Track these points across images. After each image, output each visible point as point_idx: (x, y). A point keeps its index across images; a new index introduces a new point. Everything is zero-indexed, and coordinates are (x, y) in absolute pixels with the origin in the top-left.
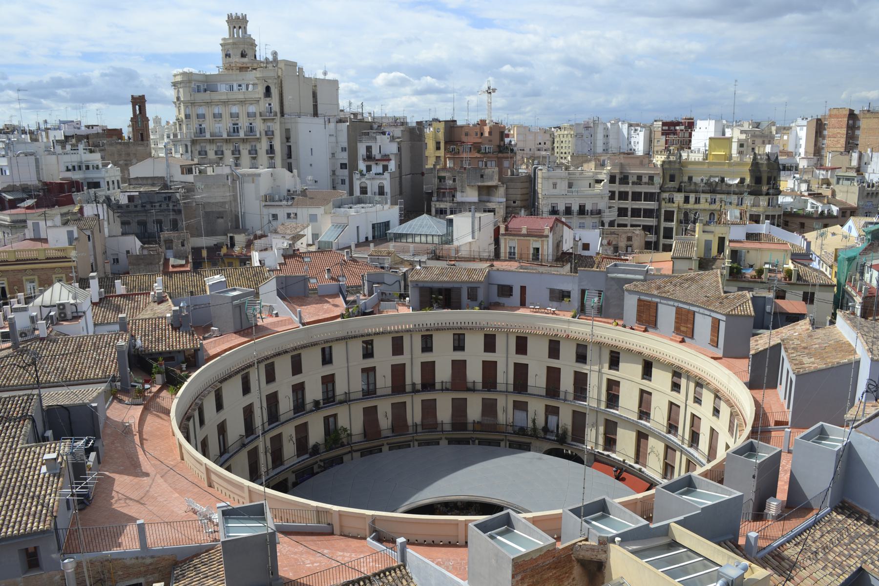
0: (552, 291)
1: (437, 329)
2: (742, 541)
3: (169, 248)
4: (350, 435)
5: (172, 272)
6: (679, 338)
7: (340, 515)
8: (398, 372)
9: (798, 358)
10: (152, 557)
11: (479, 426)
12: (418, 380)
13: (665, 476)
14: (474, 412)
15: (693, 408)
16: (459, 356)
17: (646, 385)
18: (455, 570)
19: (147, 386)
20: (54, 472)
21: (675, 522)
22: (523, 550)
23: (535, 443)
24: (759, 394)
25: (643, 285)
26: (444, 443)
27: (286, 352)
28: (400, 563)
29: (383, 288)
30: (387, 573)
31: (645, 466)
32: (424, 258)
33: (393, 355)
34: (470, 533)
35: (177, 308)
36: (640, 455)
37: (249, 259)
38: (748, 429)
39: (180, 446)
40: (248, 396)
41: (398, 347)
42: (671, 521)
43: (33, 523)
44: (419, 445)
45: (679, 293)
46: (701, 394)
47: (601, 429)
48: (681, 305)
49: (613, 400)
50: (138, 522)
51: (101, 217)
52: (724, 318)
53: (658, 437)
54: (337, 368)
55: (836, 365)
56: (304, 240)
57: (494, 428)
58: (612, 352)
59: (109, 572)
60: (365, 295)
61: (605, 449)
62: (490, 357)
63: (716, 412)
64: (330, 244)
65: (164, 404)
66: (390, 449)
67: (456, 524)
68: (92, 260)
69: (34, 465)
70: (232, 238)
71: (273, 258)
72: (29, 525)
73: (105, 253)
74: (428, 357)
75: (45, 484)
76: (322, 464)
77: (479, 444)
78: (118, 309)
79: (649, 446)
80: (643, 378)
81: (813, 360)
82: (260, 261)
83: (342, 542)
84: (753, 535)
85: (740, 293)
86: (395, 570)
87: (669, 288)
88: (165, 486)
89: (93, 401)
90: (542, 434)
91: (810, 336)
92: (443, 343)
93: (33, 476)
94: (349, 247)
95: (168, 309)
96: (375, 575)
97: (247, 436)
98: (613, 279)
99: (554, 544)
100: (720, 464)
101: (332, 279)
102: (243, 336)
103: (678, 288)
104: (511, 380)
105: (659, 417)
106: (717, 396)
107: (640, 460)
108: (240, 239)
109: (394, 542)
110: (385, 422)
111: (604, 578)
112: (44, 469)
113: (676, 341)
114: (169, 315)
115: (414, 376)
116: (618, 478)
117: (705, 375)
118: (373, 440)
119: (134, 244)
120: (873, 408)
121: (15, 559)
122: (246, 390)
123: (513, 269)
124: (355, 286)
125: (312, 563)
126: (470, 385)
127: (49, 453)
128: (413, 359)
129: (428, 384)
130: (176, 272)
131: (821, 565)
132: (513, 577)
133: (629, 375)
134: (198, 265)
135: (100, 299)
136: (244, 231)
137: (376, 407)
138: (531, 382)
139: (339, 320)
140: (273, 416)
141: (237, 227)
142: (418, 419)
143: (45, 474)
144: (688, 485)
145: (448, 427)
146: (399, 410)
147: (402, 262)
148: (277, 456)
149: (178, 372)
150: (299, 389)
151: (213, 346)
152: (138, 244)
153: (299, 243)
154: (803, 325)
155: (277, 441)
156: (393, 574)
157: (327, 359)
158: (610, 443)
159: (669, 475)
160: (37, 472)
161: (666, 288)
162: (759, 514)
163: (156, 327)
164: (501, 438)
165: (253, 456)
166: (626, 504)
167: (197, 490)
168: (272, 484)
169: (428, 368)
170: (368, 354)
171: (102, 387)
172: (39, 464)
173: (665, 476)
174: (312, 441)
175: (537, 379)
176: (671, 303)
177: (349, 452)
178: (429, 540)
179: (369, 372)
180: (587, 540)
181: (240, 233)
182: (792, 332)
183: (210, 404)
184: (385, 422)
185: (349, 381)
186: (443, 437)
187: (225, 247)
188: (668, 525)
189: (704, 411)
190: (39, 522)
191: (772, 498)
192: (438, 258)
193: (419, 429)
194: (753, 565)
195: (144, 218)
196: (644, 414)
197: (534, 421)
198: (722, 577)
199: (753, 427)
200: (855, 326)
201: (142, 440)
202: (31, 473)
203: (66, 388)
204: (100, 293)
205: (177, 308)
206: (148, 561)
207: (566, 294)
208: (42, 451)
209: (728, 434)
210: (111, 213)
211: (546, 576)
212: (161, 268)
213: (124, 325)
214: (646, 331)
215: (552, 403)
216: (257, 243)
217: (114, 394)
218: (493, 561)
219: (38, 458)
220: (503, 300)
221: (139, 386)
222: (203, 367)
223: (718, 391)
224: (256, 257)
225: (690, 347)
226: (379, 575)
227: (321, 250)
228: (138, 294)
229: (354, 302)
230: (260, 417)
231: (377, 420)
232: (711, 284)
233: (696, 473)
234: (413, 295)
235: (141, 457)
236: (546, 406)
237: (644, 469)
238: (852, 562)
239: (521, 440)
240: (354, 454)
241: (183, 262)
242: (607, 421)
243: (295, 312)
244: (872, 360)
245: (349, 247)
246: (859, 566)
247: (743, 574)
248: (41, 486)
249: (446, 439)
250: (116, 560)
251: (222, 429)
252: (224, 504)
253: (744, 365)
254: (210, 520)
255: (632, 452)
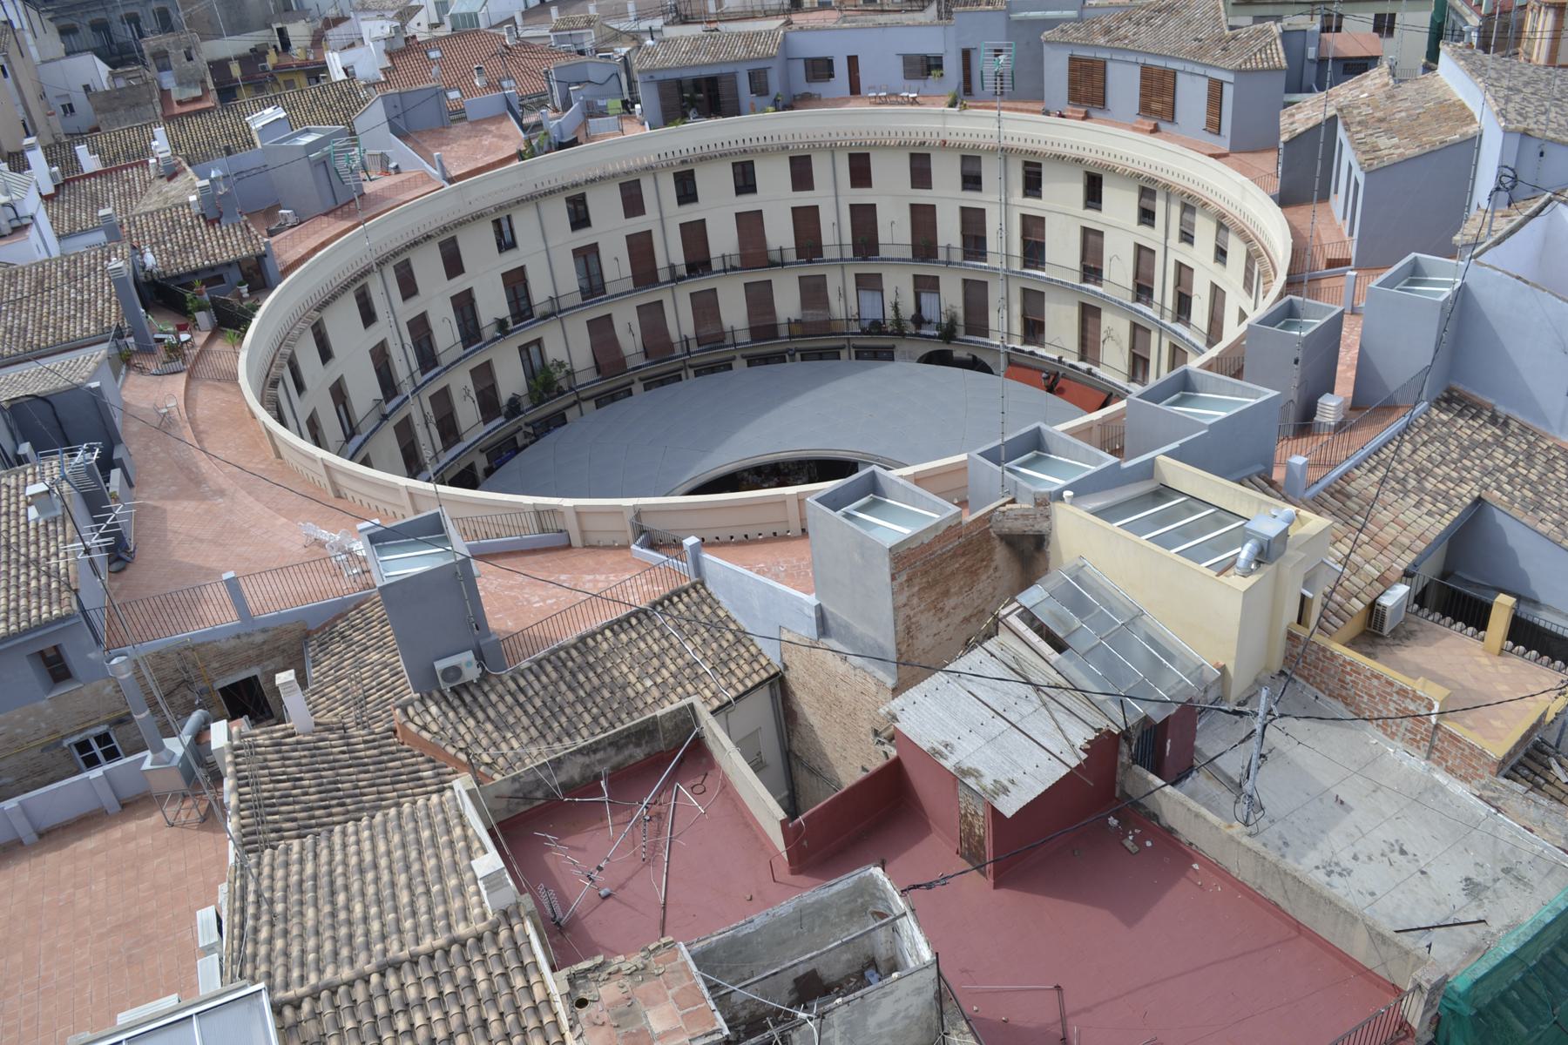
0: (908, 60)
1: (702, 159)
2: (1278, 475)
3: (164, 68)
4: (571, 373)
5: (181, 115)
6: (1149, 124)
7: (577, 513)
8: (640, 247)
9: (1368, 140)
10: (264, 631)
11: (800, 328)
12: (678, 257)
13: (1133, 378)
14: (787, 304)
15: (1179, 252)
16: (747, 203)
17: (1092, 219)
18: (790, 578)
19: (184, 337)
20: (53, 514)
21: (1165, 454)
22: (907, 531)
23: (902, 346)
24: (1302, 214)
25: (1077, 29)
26: (740, 365)
27: (428, 237)
28: (694, 579)
29: (588, 89)
30: (676, 599)
31: (1097, 363)
32: (658, 23)
33: (627, 216)
34: (809, 514)
35: (206, 182)
36: (1088, 345)
37: (324, 68)
38: (1282, 277)
39: (270, 433)
40: (373, 328)
41: (633, 202)
42: (1158, 454)
43: (39, 608)
44: (697, 374)
45: (1145, 37)
46: (1192, 225)
47: (1017, 309)
48: (1150, 61)
49: (1034, 252)
50: (226, 576)
51: (17, 25)
52: (1230, 78)
53: (1119, 307)
54: (528, 254)
55: (1438, 146)
56: (421, 17)
57: (826, 328)
58: (1026, 164)
59: (195, 666)
60: (556, 110)
61: (1026, 342)
62: (804, 199)
63: (1221, 254)
64: (472, 18)
65: (223, 364)
66: (647, 388)
67: (782, 501)
68: (21, 114)
69: (13, 508)
70: (281, 32)
71: (369, 62)
72: (34, 612)
73: (43, 96)
74: (690, 213)
75: (42, 539)
76: (530, 430)
77: (803, 359)
78: (96, 202)
79: (1104, 327)
80: (1087, 206)
81: (1396, 140)
82: (345, 70)
83: (589, 560)
84: (1299, 460)
85: (1259, 26)
86: (686, 592)
87: (1128, 29)
88: (258, 507)
89: (91, 379)
90: (911, 329)
91: (1390, 97)
92: (715, 184)
93: (17, 528)
94: (512, 20)
95: (189, 189)
96: (654, 606)
97: (388, 400)
98: (1020, 22)
99: (959, 515)
100: (1236, 345)
101: (490, 86)
102: (342, 218)
103: (1143, 28)
104: (848, 238)
105: (1119, 271)
106: (1222, 227)
107: (1089, 355)
108: (299, 32)
109: (680, 546)
110: (630, 341)
111: (1047, 560)
112: (33, 512)
113: (1142, 131)
114: (193, 198)
115: (670, 252)
116: (1050, 390)
117: (1198, 189)
118: (613, 380)
119: (96, 71)
120: (1505, 220)
121: (28, 674)
122: (368, 317)
123: (829, 24)
124: (535, 95)
125: (544, 601)
126: (775, 257)
127: (35, 482)
128: (664, 218)
129: (699, 263)
130: (189, 114)
131: (1412, 500)
132: (893, 578)
133: (1061, 203)
134: (227, 93)
135: (57, 187)
136: (303, 13)
137: (609, 316)
138: (883, 236)
139: (517, 163)
140: (427, 358)
141: (288, 9)
142: (689, 329)
143: (37, 521)
144: (1184, 387)
145: (743, 337)
146: (652, 316)
147: (618, 36)
148: (449, 430)
149: (235, 301)
150: (464, 304)
151: (286, 247)
152: (103, 69)
153: (413, 23)
154: (1375, 79)
155: (442, 400)
156: (686, 599)
157: (506, 243)
158: (1034, 329)
159: (1140, 374)
160: (22, 520)
161: (1122, 32)
162: (1305, 423)
163: (174, 225)
164: (840, 343)
165: (405, 432)
166: (1075, 433)
167: (317, 506)
168: (448, 477)
169: (695, 234)
170: (580, 219)
171: (101, 351)
172: (22, 505)
173: (1133, 378)
174: (505, 395)
175: (894, 231)
176: (1132, 58)
177: (575, 403)
178: (739, 535)
179: (587, 256)
180: (1013, 501)
181: (295, 21)
182: (1356, 92)
183: (308, 355)
184: (630, 341)
185: (553, 277)
186: (738, 355)
187: (272, 52)
188: (1153, 460)
189: (1199, 256)
190: (50, 604)
191: (1328, 395)
192: (685, 20)
193: (694, 347)
194: (1303, 513)
195: (102, 15)
196: (1092, 271)
197: (896, 307)
198: (1251, 537)
199: (1289, 275)
200: (1476, 71)
201: (198, 434)
202: (13, 523)
203: (33, 363)
204: (53, 176)
205: (206, 182)
206: (259, 638)
207: (932, 62)
208: (21, 482)
209: (1244, 293)
210: (33, 13)
211: (949, 570)
212: (159, 110)
213: (113, 231)
214: (1086, 117)
215: (926, 270)
216: (334, 34)
217: (124, 361)
218: (857, 557)
219: (17, 496)
220: (817, 88)
221: (170, 338)
222: (280, 287)
223: (1224, 216)
224: (335, 63)
225: (1170, 138)
226: (661, 604)
227: (457, 33)
228: (126, 167)
229: (538, 125)
230: (403, 363)
231: (615, 339)
232: (1204, 13)
233: (1194, 364)
234: (648, 100)
235: (204, 465)
236: (915, 276)
237: (1095, 370)
238: (1464, 489)
239: (876, 343)
240: (585, 405)
241: (199, 92)
242: (1025, 291)
243: (431, 162)
244: (1506, 131)
245: (512, 20)
246: (1476, 494)
247: (1286, 530)
248: (37, 543)
249: (743, 357)
250: (202, 644)
251: (339, 393)
252: (367, 524)
253: (1269, 163)
254: (350, 552)
255: (1073, 343)
